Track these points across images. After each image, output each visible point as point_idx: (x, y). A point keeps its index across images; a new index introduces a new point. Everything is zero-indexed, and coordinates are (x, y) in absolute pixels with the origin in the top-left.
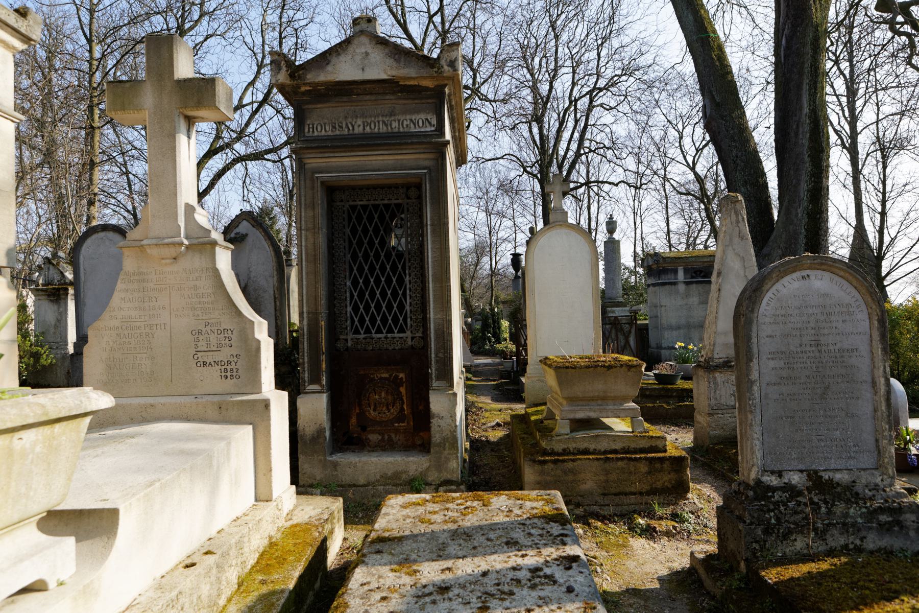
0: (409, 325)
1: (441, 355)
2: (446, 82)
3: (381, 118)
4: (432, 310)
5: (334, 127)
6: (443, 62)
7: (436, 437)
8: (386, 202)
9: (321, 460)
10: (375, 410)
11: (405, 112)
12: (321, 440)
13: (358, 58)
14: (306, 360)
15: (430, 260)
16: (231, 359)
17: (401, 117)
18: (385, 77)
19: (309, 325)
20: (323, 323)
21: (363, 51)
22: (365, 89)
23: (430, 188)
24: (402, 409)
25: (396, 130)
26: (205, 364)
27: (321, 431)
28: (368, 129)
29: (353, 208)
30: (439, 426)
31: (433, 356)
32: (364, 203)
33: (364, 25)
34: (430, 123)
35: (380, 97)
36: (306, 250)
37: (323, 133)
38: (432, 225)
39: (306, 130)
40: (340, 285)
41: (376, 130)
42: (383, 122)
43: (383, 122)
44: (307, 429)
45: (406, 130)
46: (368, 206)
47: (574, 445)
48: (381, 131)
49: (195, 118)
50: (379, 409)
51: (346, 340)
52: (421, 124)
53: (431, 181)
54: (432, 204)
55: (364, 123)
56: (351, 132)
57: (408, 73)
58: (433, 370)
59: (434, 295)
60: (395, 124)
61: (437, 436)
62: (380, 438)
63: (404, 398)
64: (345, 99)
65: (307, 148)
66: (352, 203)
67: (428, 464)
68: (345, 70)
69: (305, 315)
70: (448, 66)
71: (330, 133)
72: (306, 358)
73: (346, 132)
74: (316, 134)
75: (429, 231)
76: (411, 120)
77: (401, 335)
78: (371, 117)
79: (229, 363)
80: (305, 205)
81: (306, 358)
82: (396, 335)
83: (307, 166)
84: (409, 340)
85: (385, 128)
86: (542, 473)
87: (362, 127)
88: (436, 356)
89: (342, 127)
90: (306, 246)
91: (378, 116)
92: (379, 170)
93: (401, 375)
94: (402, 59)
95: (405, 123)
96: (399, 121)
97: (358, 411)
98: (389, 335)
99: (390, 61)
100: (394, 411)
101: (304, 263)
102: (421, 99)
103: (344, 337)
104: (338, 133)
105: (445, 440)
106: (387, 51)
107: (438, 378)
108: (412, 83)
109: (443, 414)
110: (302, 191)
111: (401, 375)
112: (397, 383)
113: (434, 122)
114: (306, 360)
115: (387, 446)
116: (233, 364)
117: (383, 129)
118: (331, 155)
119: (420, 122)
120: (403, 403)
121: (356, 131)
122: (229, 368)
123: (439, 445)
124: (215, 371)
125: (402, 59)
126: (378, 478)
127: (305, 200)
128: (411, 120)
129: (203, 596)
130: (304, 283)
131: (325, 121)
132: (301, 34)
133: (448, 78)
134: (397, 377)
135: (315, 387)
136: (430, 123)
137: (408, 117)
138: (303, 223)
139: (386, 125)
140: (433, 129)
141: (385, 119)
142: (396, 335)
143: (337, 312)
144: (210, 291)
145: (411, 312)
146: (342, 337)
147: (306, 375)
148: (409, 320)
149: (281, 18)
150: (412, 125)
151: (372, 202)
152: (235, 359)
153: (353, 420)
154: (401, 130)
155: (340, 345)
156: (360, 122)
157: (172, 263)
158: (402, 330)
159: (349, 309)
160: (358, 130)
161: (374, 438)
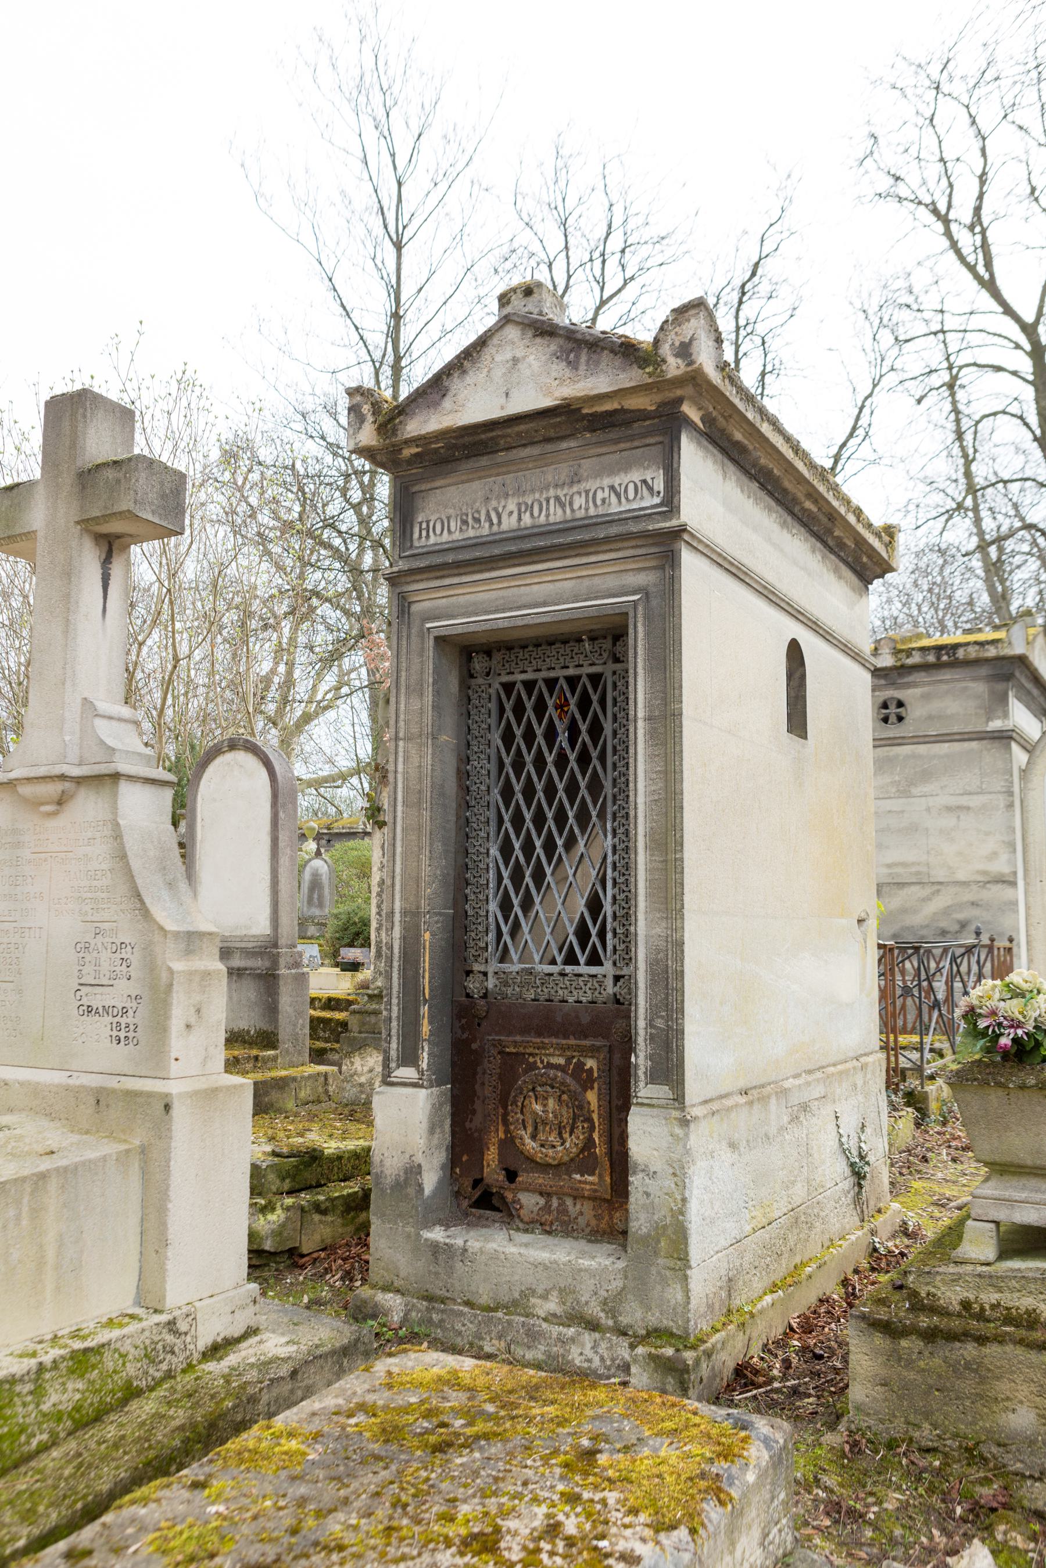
0: (610, 948)
1: (660, 1023)
2: (679, 392)
3: (552, 492)
4: (641, 916)
5: (465, 522)
6: (665, 350)
7: (640, 1222)
8: (571, 672)
9: (409, 1236)
10: (534, 1137)
11: (598, 474)
12: (411, 1191)
13: (498, 373)
14: (394, 1014)
15: (641, 800)
16: (128, 1005)
17: (591, 485)
18: (547, 402)
19: (404, 938)
20: (427, 936)
21: (509, 356)
22: (519, 434)
23: (648, 634)
24: (589, 1143)
25: (581, 514)
26: (90, 1010)
27: (413, 1171)
28: (527, 519)
29: (508, 687)
30: (648, 1194)
31: (641, 1024)
32: (529, 676)
33: (518, 304)
34: (650, 489)
35: (549, 447)
36: (406, 780)
37: (445, 537)
38: (649, 719)
39: (416, 535)
40: (479, 853)
41: (543, 518)
42: (557, 498)
43: (557, 498)
44: (388, 1163)
45: (601, 511)
46: (535, 682)
47: (994, 1297)
48: (552, 519)
49: (119, 537)
50: (542, 1137)
51: (485, 974)
52: (631, 494)
53: (648, 618)
54: (650, 670)
55: (519, 505)
56: (495, 528)
57: (598, 382)
58: (641, 1059)
59: (650, 882)
60: (579, 501)
61: (643, 1216)
62: (542, 1201)
63: (595, 1116)
64: (484, 461)
65: (412, 572)
66: (505, 679)
67: (619, 1284)
68: (475, 404)
69: (397, 917)
70: (676, 356)
71: (457, 536)
72: (395, 1009)
73: (486, 531)
74: (433, 540)
75: (641, 732)
76: (612, 488)
77: (593, 970)
78: (533, 491)
79: (125, 1011)
80: (407, 687)
81: (395, 1009)
82: (583, 969)
83: (415, 608)
84: (609, 982)
85: (559, 511)
86: (895, 1356)
87: (515, 515)
88: (650, 1024)
89: (477, 520)
90: (406, 773)
91: (547, 488)
92: (545, 604)
93: (590, 1063)
94: (584, 358)
95: (600, 495)
96: (587, 492)
97: (501, 1135)
98: (569, 969)
99: (559, 368)
100: (572, 1143)
101: (399, 808)
102: (631, 438)
103: (482, 968)
104: (471, 533)
105: (660, 1230)
106: (553, 347)
107: (654, 1078)
108: (608, 406)
109: (657, 1165)
110: (403, 659)
111: (590, 1063)
112: (586, 1081)
113: (659, 485)
114: (394, 1014)
115: (552, 1225)
116: (131, 1013)
117: (557, 515)
118: (456, 580)
119: (631, 487)
120: (592, 1128)
121: (505, 526)
122: (123, 1021)
123: (645, 1240)
124: (101, 1026)
125: (584, 358)
126: (517, 1295)
127: (408, 678)
128: (612, 488)
129: (1011, 1416)
130: (399, 850)
131: (451, 515)
132: (772, 344)
133: (679, 382)
134: (580, 1065)
135: (408, 1073)
136: (650, 489)
137: (606, 482)
138: (402, 724)
139: (563, 506)
140: (657, 500)
141: (560, 493)
142: (583, 969)
143: (470, 912)
144: (105, 866)
145: (615, 917)
146: (477, 967)
147: (394, 1045)
148: (609, 936)
149: (737, 318)
150: (614, 499)
151: (544, 674)
152: (134, 1005)
153: (492, 1155)
154: (592, 512)
155: (473, 985)
156: (512, 505)
157: (55, 814)
158: (594, 960)
159: (493, 907)
160: (509, 523)
161: (529, 1202)
